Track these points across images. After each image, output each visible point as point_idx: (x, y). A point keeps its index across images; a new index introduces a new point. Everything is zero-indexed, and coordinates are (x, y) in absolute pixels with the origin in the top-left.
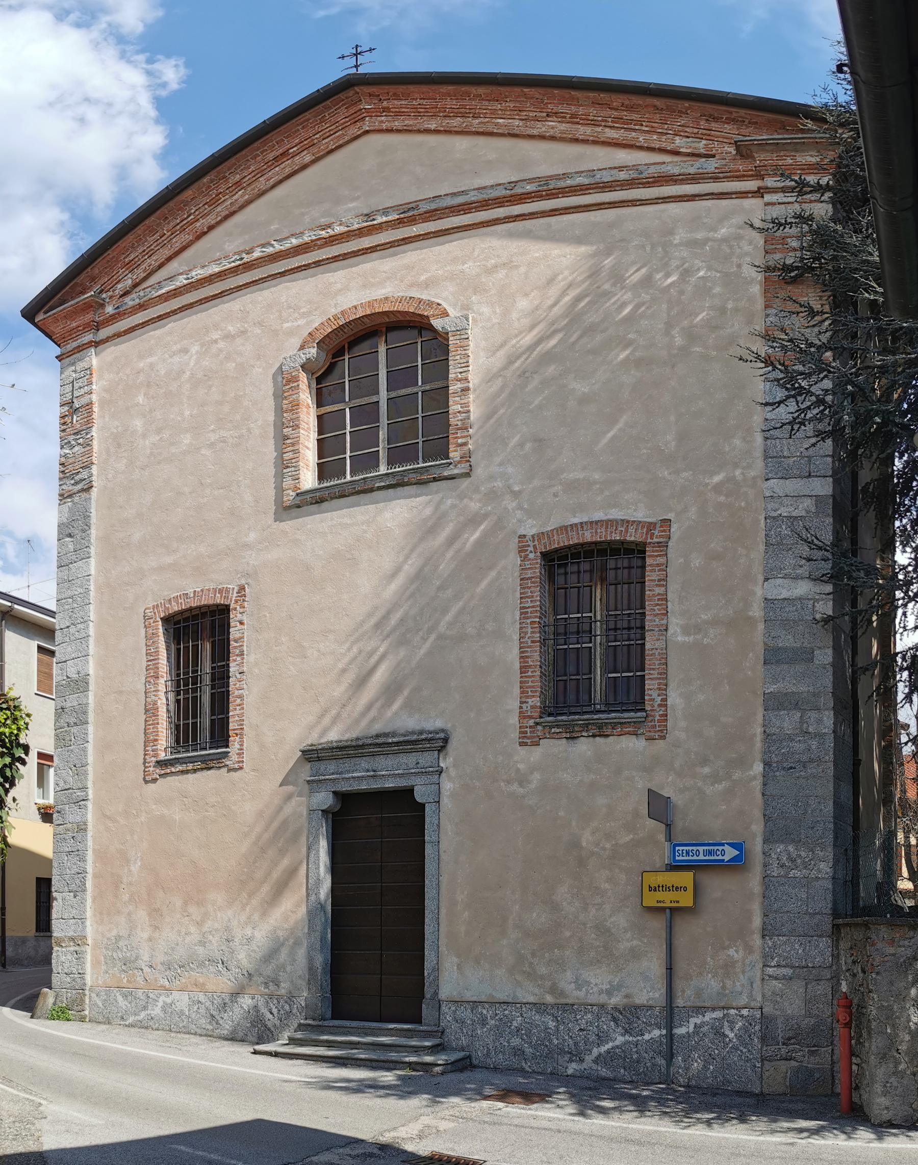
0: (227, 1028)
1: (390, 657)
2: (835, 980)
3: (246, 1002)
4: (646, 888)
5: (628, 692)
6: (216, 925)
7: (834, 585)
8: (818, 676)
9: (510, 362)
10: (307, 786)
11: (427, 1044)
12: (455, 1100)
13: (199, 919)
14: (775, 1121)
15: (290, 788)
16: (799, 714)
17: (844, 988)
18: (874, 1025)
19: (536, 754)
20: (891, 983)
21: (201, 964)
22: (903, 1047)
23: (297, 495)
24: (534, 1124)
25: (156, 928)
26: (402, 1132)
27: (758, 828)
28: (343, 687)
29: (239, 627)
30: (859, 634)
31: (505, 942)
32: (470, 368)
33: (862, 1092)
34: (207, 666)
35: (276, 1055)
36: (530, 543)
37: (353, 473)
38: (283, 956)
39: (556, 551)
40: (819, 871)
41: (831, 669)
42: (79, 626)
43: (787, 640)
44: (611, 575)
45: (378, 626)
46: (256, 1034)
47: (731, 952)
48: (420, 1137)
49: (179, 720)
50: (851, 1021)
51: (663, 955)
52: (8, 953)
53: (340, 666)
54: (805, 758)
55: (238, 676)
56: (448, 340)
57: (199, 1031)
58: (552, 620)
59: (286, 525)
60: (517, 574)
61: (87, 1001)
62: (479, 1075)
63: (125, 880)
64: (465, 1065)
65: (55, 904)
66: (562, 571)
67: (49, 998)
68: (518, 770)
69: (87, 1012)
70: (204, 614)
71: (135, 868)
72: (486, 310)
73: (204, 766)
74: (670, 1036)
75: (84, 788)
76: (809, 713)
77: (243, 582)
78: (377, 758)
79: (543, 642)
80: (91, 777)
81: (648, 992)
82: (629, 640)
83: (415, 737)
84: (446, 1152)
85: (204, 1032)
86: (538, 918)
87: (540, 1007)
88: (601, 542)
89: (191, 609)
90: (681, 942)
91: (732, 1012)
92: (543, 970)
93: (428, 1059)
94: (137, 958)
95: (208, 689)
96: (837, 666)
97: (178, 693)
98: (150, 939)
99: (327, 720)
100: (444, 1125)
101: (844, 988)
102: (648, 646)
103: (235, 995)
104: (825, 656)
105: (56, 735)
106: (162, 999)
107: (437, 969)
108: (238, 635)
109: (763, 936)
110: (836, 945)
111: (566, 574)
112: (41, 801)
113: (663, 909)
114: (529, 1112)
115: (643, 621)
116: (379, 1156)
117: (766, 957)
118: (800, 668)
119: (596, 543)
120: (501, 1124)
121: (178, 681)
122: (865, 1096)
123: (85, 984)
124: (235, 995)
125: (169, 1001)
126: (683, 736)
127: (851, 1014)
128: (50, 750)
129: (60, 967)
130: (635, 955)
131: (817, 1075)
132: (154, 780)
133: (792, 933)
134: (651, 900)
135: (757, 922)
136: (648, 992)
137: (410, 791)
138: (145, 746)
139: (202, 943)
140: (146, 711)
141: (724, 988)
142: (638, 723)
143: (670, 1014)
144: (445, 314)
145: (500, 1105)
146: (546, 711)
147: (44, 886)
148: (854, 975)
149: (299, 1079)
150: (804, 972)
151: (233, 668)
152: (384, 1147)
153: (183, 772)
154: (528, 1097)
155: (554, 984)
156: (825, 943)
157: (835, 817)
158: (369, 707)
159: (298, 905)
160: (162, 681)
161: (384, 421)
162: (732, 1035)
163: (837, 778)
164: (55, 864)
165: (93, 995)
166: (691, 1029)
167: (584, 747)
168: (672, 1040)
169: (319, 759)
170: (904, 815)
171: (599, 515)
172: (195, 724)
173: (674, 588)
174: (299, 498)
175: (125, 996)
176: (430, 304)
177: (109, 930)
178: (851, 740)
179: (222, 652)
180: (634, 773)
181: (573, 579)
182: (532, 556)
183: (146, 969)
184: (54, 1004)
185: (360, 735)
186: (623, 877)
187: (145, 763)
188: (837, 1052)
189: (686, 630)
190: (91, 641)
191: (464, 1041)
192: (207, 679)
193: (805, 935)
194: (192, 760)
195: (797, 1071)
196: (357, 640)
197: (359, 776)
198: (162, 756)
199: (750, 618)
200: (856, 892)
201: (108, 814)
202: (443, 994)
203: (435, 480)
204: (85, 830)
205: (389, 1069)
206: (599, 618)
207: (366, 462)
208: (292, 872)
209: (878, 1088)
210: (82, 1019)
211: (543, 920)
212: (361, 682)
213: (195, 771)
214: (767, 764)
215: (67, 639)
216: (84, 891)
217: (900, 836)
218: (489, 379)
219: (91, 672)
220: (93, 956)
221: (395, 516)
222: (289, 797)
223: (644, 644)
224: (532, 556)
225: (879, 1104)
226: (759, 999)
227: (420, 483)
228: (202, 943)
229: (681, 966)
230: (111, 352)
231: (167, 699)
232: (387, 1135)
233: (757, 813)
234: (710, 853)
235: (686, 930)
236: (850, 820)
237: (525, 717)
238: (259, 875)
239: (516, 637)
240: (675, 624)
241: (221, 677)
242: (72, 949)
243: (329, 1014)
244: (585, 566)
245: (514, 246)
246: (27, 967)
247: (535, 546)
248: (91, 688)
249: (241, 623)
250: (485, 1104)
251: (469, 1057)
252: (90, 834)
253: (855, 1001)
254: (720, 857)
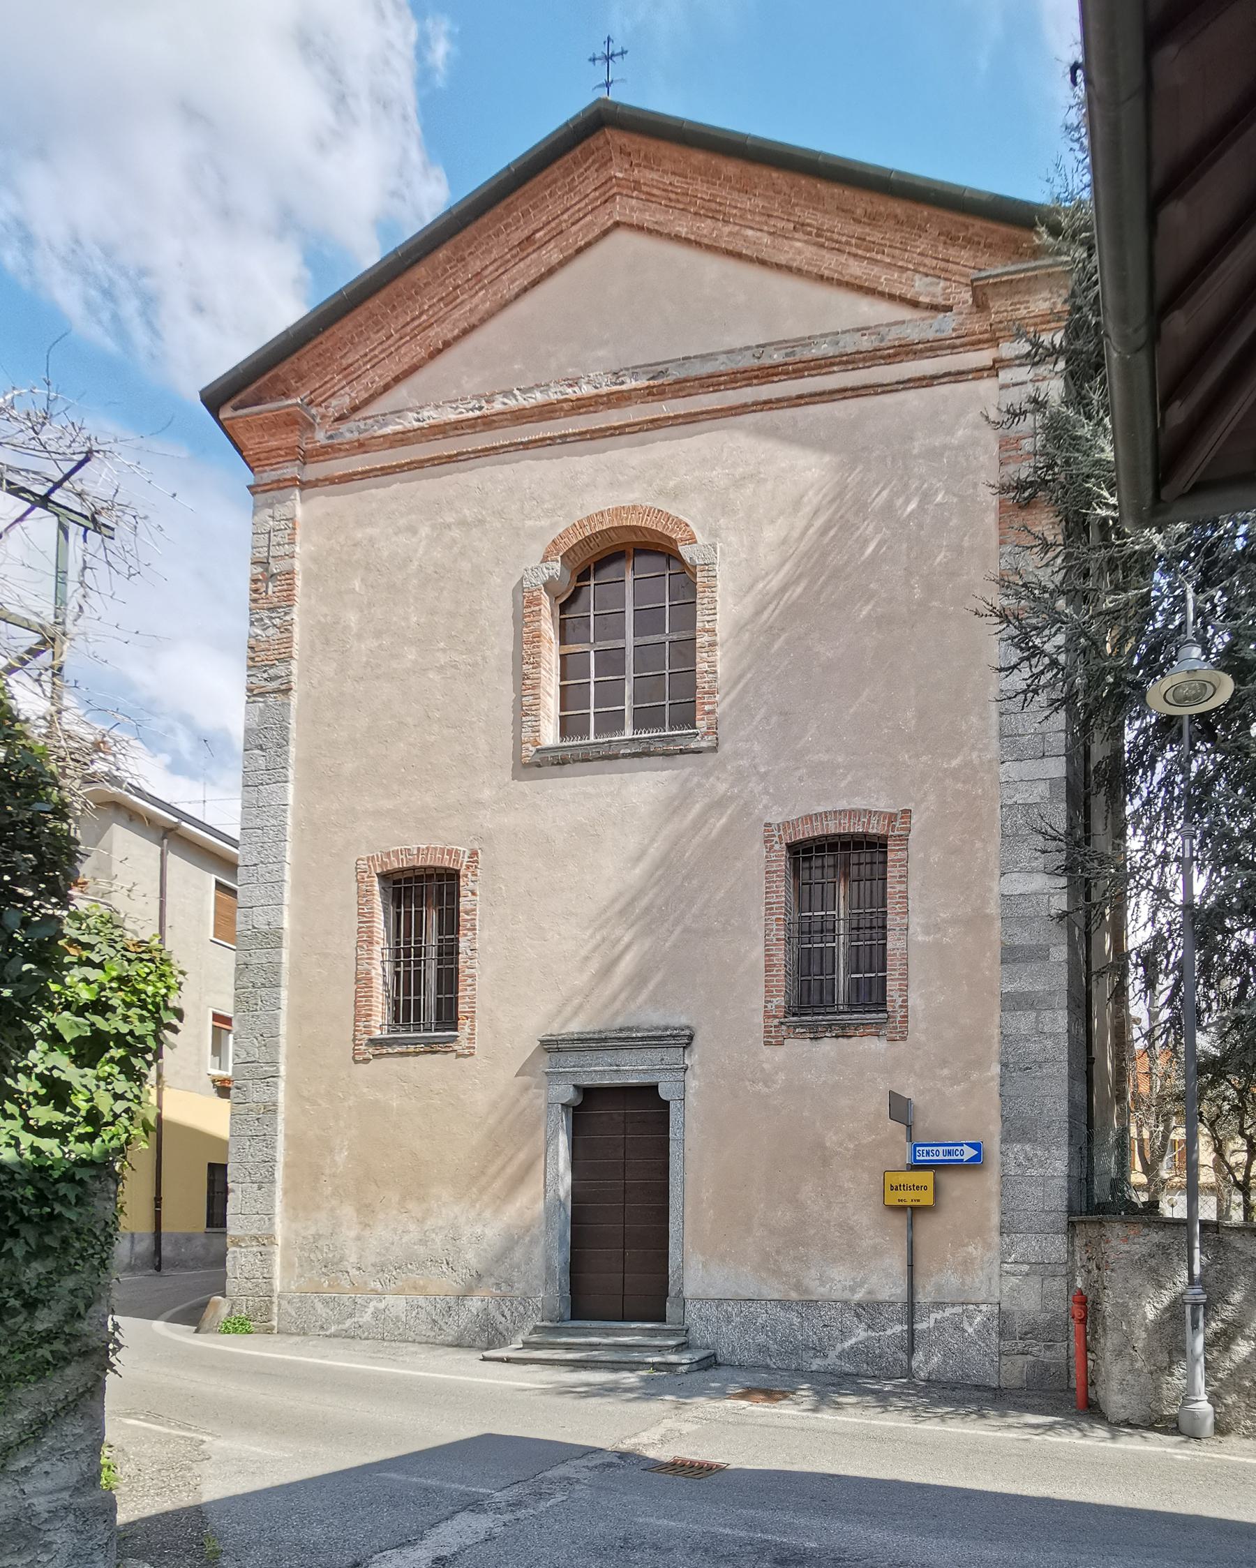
0: (451, 1333)
1: (635, 948)
2: (1070, 1276)
3: (474, 1304)
4: (888, 1188)
5: (870, 995)
6: (441, 1223)
7: (1069, 878)
8: (1052, 976)
9: (758, 613)
10: (546, 1078)
11: (671, 1343)
12: (701, 1400)
13: (420, 1215)
14: (1003, 1415)
15: (526, 1079)
16: (1034, 1014)
17: (1079, 1284)
18: (1109, 1321)
19: (778, 1055)
20: (1126, 1280)
21: (422, 1265)
22: (1139, 1345)
23: (538, 751)
24: (777, 1422)
25: (367, 1225)
26: (644, 1438)
27: (995, 1128)
28: (585, 977)
29: (471, 897)
30: (1093, 928)
31: (750, 1240)
32: (718, 617)
33: (1098, 1388)
34: (432, 939)
35: (508, 1360)
36: (775, 832)
37: (598, 733)
38: (518, 1254)
39: (801, 842)
40: (1055, 1170)
41: (1066, 966)
42: (271, 867)
43: (1023, 938)
44: (854, 870)
45: (622, 913)
46: (485, 1338)
47: (970, 1249)
48: (662, 1442)
49: (398, 994)
50: (1086, 1317)
51: (905, 1253)
52: (163, 1253)
53: (583, 952)
54: (1040, 1059)
55: (469, 953)
56: (695, 576)
57: (418, 1339)
58: (797, 916)
59: (525, 786)
60: (763, 866)
61: (275, 1309)
62: (723, 1373)
63: (327, 1171)
64: (710, 1363)
65: (230, 1196)
66: (807, 865)
67: (221, 1307)
68: (763, 1070)
69: (275, 1323)
70: (430, 877)
71: (341, 1157)
72: (733, 539)
73: (428, 1049)
74: (912, 1332)
75: (274, 1063)
76: (1044, 1013)
77: (476, 846)
78: (621, 1053)
79: (788, 941)
80: (283, 1050)
82: (871, 940)
83: (660, 1033)
84: (688, 1457)
85: (425, 1339)
86: (784, 1216)
87: (783, 1304)
88: (844, 835)
89: (414, 869)
90: (922, 1239)
91: (971, 1307)
92: (787, 1267)
93: (673, 1358)
94: (342, 1259)
95: (434, 963)
96: (1072, 964)
97: (398, 964)
98: (358, 1238)
99: (569, 1010)
100: (687, 1428)
101: (1079, 1284)
102: (889, 946)
103: (462, 1297)
104: (1060, 953)
105: (237, 996)
106: (372, 1304)
107: (681, 1268)
108: (469, 907)
109: (1001, 1234)
110: (1071, 1242)
111: (811, 868)
112: (216, 1072)
113: (903, 1208)
114: (774, 1410)
115: (884, 919)
116: (618, 1465)
117: (1004, 1254)
118: (1035, 967)
119: (839, 835)
120: (744, 1424)
121: (398, 950)
122: (1101, 1393)
123: (272, 1291)
124: (462, 1297)
125: (382, 1306)
126: (923, 1038)
127: (1086, 1310)
128: (228, 1013)
129: (239, 1271)
130: (877, 1252)
131: (1053, 1370)
132: (367, 1061)
133: (1029, 1230)
134: (893, 1198)
135: (995, 1219)
136: (891, 1289)
137: (654, 1088)
138: (356, 1021)
139: (422, 1242)
140: (357, 980)
141: (963, 1284)
142: (880, 1025)
143: (911, 1309)
144: (692, 540)
145: (744, 1403)
146: (790, 1012)
147: (217, 1173)
148: (1089, 1272)
149: (533, 1386)
150: (1041, 1269)
151: (463, 945)
152: (623, 1455)
153: (402, 1054)
154: (769, 1395)
155: (798, 1281)
156: (1060, 1241)
157: (1070, 1116)
158: (614, 997)
159: (534, 1201)
160: (377, 948)
161: (630, 674)
162: (970, 1330)
163: (1072, 1077)
164: (232, 1150)
165: (284, 1303)
166: (932, 1325)
167: (828, 1047)
168: (913, 1338)
169: (559, 1050)
170: (1137, 1109)
171: (843, 804)
172: (417, 1002)
173: (914, 884)
174: (539, 756)
175: (326, 1303)
176: (679, 522)
177: (306, 1228)
178: (1084, 1039)
179: (450, 923)
180: (876, 1075)
181: (817, 874)
182: (777, 847)
183: (353, 1272)
184: (230, 1314)
185: (602, 1028)
186: (865, 1176)
187: (354, 1040)
188: (1072, 1346)
189: (927, 930)
190: (287, 888)
191: (709, 1339)
192: (433, 953)
193: (1042, 1232)
194: (414, 1042)
195: (1034, 1365)
196: (601, 927)
197: (604, 1071)
198: (377, 1034)
199: (987, 916)
200: (1090, 1191)
201: (306, 1094)
202: (687, 1293)
203: (682, 752)
204: (275, 1111)
205: (632, 1370)
206: (842, 916)
207: (611, 722)
208: (528, 1168)
209: (1114, 1385)
210: (269, 1331)
211: (788, 1217)
212: (606, 971)
213: (417, 1054)
214: (1004, 1065)
215: (254, 879)
216: (273, 1182)
217: (1133, 1131)
218: (739, 628)
219: (286, 925)
220: (283, 1256)
221: (643, 787)
222: (526, 1088)
223: (885, 944)
224: (777, 847)
225: (1115, 1402)
226: (997, 1294)
227: (667, 754)
228: (422, 1242)
229: (922, 1263)
231: (384, 970)
232: (628, 1441)
233: (995, 1114)
234: (949, 1153)
235: (928, 1228)
236: (1084, 1118)
237: (769, 1017)
238: (492, 1170)
239: (762, 934)
240: (916, 921)
241: (449, 952)
242: (255, 1249)
243: (568, 1315)
244: (829, 861)
245: (765, 447)
246: (193, 1269)
247: (780, 836)
248: (284, 944)
249: (474, 894)
250: (729, 1403)
251: (714, 1355)
252: (281, 1117)
253: (1090, 1297)
254: (959, 1157)
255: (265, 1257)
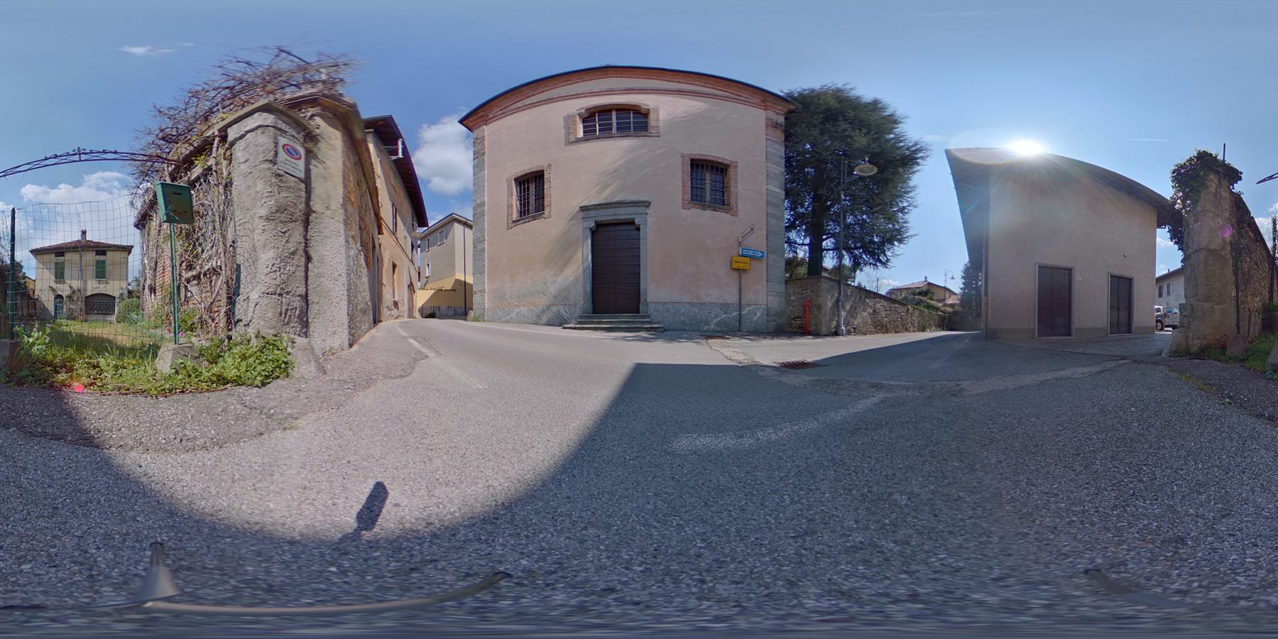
3: (555, 309)
19: (689, 212)
67: (472, 314)
81: (732, 298)
87: (692, 304)
134: (735, 266)
136: (732, 298)
202: (649, 300)
230: (491, 125)
255: (483, 297)
